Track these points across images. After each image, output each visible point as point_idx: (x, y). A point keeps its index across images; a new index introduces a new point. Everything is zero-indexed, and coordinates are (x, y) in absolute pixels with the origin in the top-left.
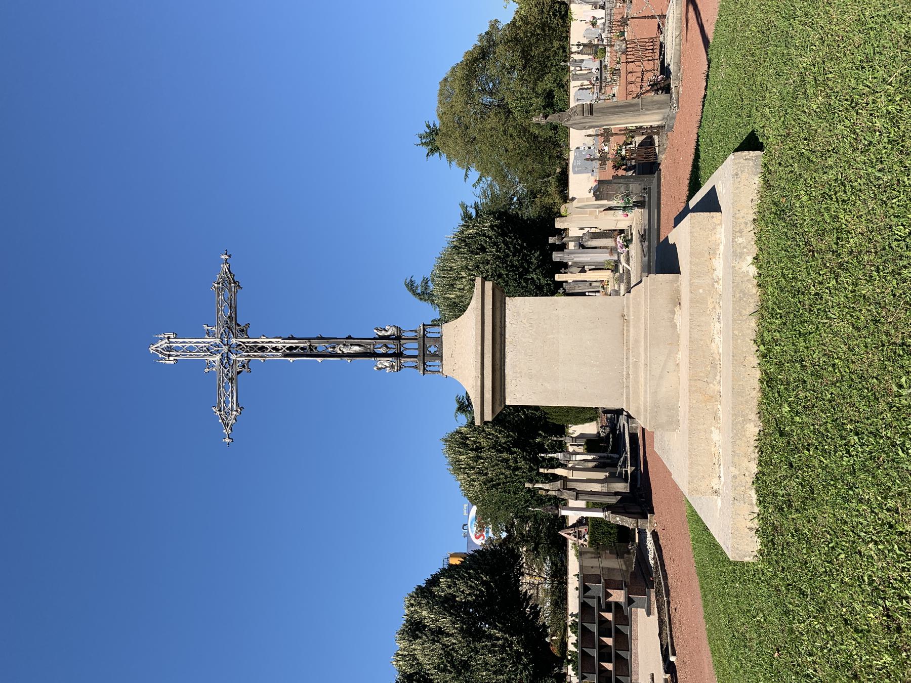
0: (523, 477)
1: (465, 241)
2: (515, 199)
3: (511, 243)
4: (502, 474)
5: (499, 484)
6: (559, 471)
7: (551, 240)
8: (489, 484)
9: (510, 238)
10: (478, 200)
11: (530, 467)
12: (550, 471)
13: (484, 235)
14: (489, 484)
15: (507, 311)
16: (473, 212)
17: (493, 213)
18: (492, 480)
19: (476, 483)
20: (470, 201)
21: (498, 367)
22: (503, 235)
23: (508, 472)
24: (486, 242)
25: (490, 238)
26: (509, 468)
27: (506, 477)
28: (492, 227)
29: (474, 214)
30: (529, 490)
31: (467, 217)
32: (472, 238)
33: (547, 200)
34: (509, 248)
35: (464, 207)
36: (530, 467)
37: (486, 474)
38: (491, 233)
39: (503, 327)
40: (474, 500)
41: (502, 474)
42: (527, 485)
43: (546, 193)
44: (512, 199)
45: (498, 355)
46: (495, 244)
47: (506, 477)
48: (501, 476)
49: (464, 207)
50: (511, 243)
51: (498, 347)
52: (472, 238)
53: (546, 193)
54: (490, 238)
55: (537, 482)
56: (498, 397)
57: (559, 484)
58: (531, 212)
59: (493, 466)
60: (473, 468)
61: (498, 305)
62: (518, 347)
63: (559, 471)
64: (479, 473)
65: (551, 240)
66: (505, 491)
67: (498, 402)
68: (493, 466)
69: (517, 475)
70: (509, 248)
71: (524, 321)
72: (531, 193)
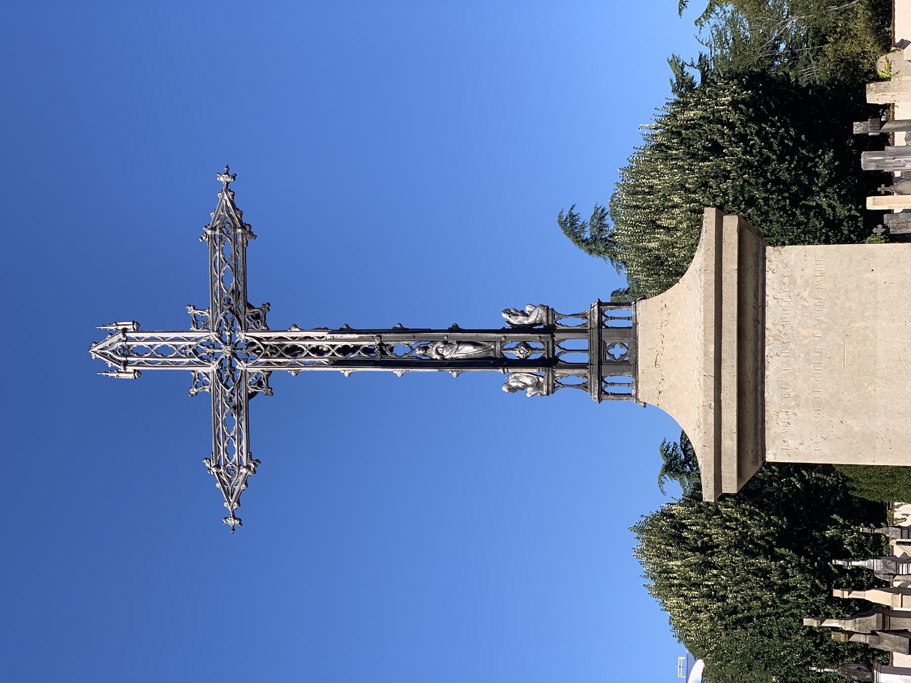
0: (798, 607)
1: (679, 134)
2: (783, 46)
3: (774, 136)
4: (757, 598)
5: (750, 619)
6: (874, 596)
7: (858, 128)
8: (729, 619)
9: (773, 125)
10: (706, 51)
11: (814, 585)
12: (856, 595)
13: (719, 121)
14: (729, 619)
15: (769, 275)
16: (696, 76)
17: (737, 76)
18: (735, 611)
19: (702, 616)
20: (690, 53)
21: (749, 386)
22: (759, 119)
23: (767, 596)
24: (723, 134)
25: (732, 126)
26: (770, 586)
27: (764, 605)
28: (734, 104)
29: (698, 80)
30: (811, 631)
31: (683, 85)
32: (693, 127)
33: (849, 48)
34: (770, 146)
35: (678, 65)
36: (814, 585)
37: (724, 598)
38: (733, 117)
39: (761, 306)
40: (697, 649)
41: (757, 598)
42: (807, 622)
43: (846, 34)
44: (776, 47)
45: (749, 363)
46: (743, 138)
47: (764, 605)
48: (754, 603)
49: (678, 65)
50: (774, 136)
51: (749, 346)
52: (693, 127)
53: (846, 34)
54: (732, 126)
55: (828, 616)
56: (749, 446)
57: (873, 620)
58: (815, 72)
59: (737, 584)
60: (697, 585)
61: (750, 262)
62: (792, 346)
63: (874, 596)
64: (709, 596)
65: (858, 128)
66: (762, 633)
67: (749, 457)
68: (737, 584)
69: (786, 602)
70: (770, 146)
71: (805, 294)
72: (817, 31)
